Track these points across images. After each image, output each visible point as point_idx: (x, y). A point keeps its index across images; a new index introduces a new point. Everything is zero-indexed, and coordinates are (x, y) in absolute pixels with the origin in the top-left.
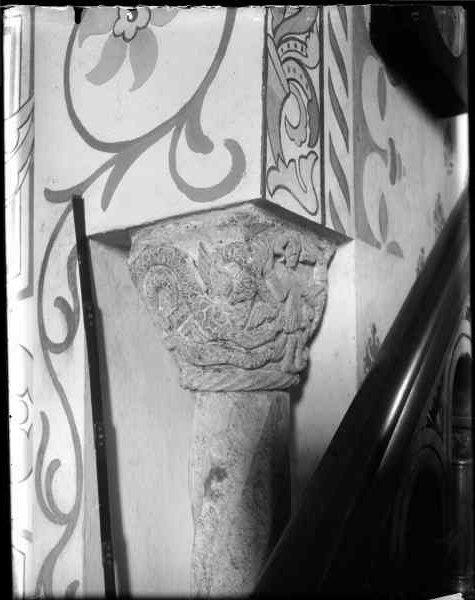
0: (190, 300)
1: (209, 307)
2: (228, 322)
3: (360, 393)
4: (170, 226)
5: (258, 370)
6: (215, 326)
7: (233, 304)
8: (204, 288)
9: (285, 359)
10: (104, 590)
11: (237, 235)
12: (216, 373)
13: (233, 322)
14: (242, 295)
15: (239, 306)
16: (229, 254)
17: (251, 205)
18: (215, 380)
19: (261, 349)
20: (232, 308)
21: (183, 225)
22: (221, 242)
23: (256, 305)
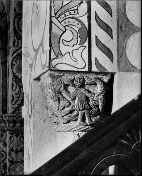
19: (66, 117)
23: (61, 102)
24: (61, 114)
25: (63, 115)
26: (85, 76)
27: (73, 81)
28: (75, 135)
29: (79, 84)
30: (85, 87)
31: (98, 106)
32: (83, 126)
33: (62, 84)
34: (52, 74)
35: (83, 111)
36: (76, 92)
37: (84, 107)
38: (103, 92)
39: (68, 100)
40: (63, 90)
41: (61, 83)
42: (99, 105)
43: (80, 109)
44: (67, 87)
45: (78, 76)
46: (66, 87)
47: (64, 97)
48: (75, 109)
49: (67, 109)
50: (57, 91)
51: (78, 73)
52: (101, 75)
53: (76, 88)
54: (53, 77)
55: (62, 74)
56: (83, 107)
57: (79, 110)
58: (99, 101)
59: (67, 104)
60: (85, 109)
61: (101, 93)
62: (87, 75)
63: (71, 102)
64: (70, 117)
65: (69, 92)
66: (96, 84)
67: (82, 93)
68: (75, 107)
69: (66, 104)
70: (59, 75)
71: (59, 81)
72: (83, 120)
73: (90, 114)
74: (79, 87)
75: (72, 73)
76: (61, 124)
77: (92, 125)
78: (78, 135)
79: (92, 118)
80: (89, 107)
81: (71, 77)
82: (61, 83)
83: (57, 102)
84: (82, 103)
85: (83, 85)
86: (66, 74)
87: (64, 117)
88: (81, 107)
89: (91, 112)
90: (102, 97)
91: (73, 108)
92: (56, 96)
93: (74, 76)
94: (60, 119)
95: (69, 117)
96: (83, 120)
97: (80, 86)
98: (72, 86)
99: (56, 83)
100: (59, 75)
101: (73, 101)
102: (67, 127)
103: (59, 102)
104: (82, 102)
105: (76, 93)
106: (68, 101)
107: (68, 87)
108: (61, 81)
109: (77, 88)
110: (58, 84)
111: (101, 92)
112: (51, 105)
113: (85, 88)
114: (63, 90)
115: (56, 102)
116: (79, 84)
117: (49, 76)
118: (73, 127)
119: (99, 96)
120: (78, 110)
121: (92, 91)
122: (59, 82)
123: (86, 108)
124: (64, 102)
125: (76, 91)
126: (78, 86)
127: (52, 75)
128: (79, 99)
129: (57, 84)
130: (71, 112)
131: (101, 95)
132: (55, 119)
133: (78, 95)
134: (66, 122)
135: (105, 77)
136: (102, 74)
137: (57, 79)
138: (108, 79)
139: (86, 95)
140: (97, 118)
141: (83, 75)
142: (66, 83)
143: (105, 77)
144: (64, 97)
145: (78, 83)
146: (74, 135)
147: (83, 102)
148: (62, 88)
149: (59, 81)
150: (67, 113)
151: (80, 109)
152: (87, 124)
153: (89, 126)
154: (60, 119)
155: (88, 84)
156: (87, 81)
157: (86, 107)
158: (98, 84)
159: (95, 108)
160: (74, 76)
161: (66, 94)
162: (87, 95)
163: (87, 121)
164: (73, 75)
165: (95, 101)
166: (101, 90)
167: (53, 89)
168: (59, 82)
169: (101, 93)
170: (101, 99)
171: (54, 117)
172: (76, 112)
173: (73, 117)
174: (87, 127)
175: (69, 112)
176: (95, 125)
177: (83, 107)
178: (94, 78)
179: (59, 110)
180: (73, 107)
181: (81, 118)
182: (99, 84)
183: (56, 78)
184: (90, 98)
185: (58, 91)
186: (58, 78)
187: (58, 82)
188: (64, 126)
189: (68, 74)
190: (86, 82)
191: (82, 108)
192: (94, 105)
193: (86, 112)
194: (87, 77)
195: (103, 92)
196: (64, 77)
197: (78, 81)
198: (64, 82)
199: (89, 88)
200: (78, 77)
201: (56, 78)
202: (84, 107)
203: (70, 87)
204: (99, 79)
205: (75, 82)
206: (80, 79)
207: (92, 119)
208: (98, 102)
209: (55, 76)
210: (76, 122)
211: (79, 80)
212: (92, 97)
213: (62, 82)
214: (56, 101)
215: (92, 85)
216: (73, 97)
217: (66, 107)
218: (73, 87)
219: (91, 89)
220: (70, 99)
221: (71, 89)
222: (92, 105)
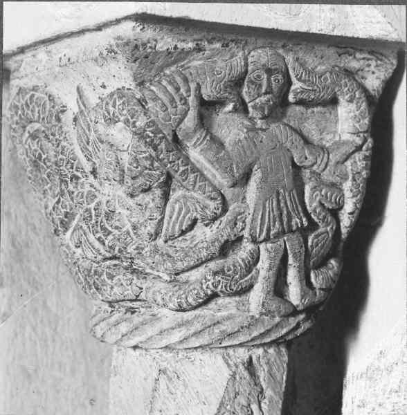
0: (71, 187)
1: (96, 200)
2: (128, 227)
3: (341, 410)
4: (41, 54)
5: (197, 312)
6: (110, 233)
7: (132, 196)
8: (88, 167)
9: (256, 287)
10: (4, 5)
11: (120, 75)
12: (129, 315)
13: (135, 228)
14: (141, 181)
15: (141, 198)
16: (111, 109)
17: (131, 24)
18: (124, 328)
19: (195, 275)
20: (131, 202)
21: (61, 49)
22: (104, 87)
23: (174, 196)
24: (174, 262)
25: (180, 266)
26: (290, 58)
27: (238, 83)
28: (234, 369)
29: (264, 99)
30: (284, 114)
31: (335, 213)
32: (277, 319)
33: (192, 100)
34: (145, 40)
35: (281, 242)
36: (252, 139)
37: (285, 219)
38: (365, 141)
39: (216, 183)
40: (195, 131)
41: (189, 90)
42: (341, 208)
43: (269, 230)
44: (210, 116)
45: (260, 56)
46: (207, 107)
47: (198, 170)
48: (246, 234)
49: (205, 235)
50: (164, 137)
51: (260, 42)
52: (358, 55)
53: (247, 123)
54: (146, 57)
55: (191, 45)
56: (281, 221)
57: (267, 240)
58: (347, 185)
59: (212, 205)
60: (291, 231)
61: (359, 148)
62: (300, 55)
63: (228, 193)
64: (218, 278)
65: (222, 145)
66: (334, 102)
67: (278, 147)
68: (248, 220)
69: (205, 207)
70: (176, 47)
71: (178, 79)
72: (279, 288)
73: (307, 254)
74: (263, 118)
75: (236, 41)
76: (156, 310)
77: (310, 310)
78: (63, 274)
79: (312, 275)
80: (336, 228)
81: (229, 61)
82: (189, 90)
83: (151, 200)
84: (278, 201)
85: (279, 106)
86: (210, 42)
87: (183, 277)
88: (274, 222)
89: (310, 244)
90: (361, 164)
91: (240, 224)
92: (156, 164)
93: (246, 59)
94: (157, 288)
95: (215, 274)
96: (279, 288)
97: (271, 110)
98: (235, 110)
99: (161, 95)
100: (176, 47)
101: (237, 190)
102: (198, 327)
103: (166, 197)
104: (278, 194)
105: (255, 145)
106: (215, 189)
107: (214, 115)
108: (186, 80)
109: (251, 119)
110: (172, 101)
111: (359, 141)
112: (104, 208)
113: (285, 121)
114: (195, 131)
115: (146, 198)
116: (264, 99)
117: (131, 47)
118: (228, 327)
119: (348, 163)
120: (262, 238)
121: (315, 137)
122: (178, 89)
123: (294, 228)
124: (195, 195)
125: (251, 134)
126: (262, 109)
127: (144, 45)
128: (264, 180)
129: (166, 100)
130: (226, 248)
131: (358, 156)
132: (121, 286)
133: (262, 160)
134: (194, 303)
135: (372, 68)
136: (361, 51)
137: (162, 69)
138: (382, 77)
139: (293, 158)
140: (330, 272)
141: (281, 51)
142: (207, 93)
143: (373, 63)
144: (195, 170)
145: (259, 96)
146: (229, 365)
147: (284, 197)
148: (190, 121)
149: (178, 79)
150: (204, 254)
151: (269, 230)
152: (295, 308)
153: (302, 317)
154: (160, 285)
155: (300, 102)
156: (297, 85)
157: (295, 221)
158: (342, 100)
159: (328, 224)
160: (246, 59)
161: (210, 154)
162: (295, 160)
163: (294, 293)
164: (240, 54)
165: (327, 186)
166: (357, 133)
167: (148, 125)
168: (178, 89)
169: (359, 148)
170: (354, 179)
171: (121, 277)
172: (247, 246)
173: (235, 272)
174: (293, 322)
175: (215, 249)
176: (321, 309)
177: (281, 221)
178: (331, 73)
179: (160, 241)
180: (236, 224)
181: (272, 280)
182: (351, 101)
183: (159, 63)
184: (306, 174)
185: (170, 138)
186: (168, 65)
187: (169, 88)
188: (180, 325)
189: (218, 45)
190: (293, 88)
191: (277, 225)
192: (321, 204)
193: (291, 243)
194: (302, 65)
195: (365, 141)
196: (196, 62)
197: (260, 86)
198: (199, 87)
199: (303, 119)
200: (264, 60)
201: (159, 63)
202: (285, 219)
203: (221, 116)
204: (349, 73)
205: (245, 89)
206: (269, 72)
207: (313, 280)
208: (341, 190)
209: (157, 53)
210: (243, 297)
211: (265, 76)
212: (315, 168)
213: (193, 86)
214: (147, 190)
215: (317, 105)
216: (241, 172)
217: (199, 224)
218: (236, 116)
219: (310, 129)
220: (221, 180)
221: (229, 127)
222: (315, 211)
